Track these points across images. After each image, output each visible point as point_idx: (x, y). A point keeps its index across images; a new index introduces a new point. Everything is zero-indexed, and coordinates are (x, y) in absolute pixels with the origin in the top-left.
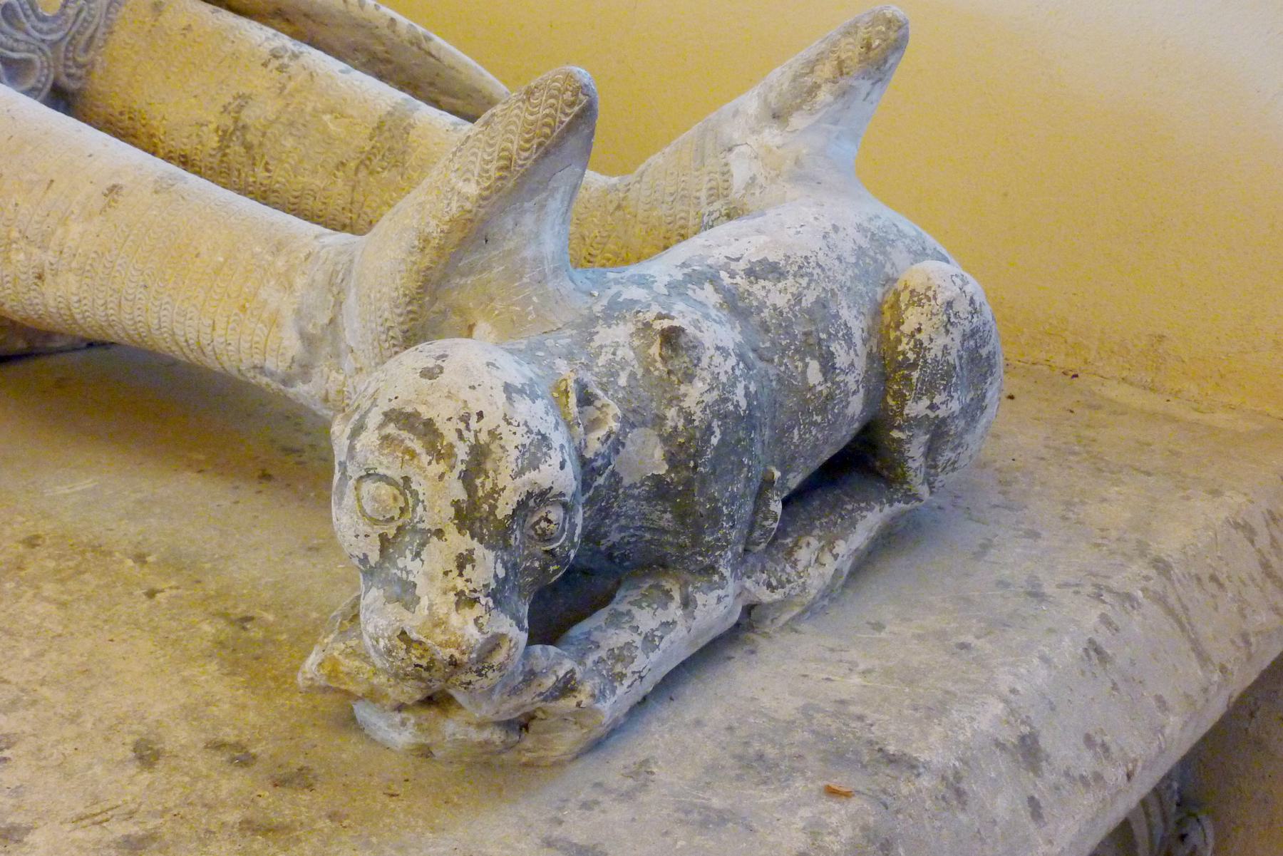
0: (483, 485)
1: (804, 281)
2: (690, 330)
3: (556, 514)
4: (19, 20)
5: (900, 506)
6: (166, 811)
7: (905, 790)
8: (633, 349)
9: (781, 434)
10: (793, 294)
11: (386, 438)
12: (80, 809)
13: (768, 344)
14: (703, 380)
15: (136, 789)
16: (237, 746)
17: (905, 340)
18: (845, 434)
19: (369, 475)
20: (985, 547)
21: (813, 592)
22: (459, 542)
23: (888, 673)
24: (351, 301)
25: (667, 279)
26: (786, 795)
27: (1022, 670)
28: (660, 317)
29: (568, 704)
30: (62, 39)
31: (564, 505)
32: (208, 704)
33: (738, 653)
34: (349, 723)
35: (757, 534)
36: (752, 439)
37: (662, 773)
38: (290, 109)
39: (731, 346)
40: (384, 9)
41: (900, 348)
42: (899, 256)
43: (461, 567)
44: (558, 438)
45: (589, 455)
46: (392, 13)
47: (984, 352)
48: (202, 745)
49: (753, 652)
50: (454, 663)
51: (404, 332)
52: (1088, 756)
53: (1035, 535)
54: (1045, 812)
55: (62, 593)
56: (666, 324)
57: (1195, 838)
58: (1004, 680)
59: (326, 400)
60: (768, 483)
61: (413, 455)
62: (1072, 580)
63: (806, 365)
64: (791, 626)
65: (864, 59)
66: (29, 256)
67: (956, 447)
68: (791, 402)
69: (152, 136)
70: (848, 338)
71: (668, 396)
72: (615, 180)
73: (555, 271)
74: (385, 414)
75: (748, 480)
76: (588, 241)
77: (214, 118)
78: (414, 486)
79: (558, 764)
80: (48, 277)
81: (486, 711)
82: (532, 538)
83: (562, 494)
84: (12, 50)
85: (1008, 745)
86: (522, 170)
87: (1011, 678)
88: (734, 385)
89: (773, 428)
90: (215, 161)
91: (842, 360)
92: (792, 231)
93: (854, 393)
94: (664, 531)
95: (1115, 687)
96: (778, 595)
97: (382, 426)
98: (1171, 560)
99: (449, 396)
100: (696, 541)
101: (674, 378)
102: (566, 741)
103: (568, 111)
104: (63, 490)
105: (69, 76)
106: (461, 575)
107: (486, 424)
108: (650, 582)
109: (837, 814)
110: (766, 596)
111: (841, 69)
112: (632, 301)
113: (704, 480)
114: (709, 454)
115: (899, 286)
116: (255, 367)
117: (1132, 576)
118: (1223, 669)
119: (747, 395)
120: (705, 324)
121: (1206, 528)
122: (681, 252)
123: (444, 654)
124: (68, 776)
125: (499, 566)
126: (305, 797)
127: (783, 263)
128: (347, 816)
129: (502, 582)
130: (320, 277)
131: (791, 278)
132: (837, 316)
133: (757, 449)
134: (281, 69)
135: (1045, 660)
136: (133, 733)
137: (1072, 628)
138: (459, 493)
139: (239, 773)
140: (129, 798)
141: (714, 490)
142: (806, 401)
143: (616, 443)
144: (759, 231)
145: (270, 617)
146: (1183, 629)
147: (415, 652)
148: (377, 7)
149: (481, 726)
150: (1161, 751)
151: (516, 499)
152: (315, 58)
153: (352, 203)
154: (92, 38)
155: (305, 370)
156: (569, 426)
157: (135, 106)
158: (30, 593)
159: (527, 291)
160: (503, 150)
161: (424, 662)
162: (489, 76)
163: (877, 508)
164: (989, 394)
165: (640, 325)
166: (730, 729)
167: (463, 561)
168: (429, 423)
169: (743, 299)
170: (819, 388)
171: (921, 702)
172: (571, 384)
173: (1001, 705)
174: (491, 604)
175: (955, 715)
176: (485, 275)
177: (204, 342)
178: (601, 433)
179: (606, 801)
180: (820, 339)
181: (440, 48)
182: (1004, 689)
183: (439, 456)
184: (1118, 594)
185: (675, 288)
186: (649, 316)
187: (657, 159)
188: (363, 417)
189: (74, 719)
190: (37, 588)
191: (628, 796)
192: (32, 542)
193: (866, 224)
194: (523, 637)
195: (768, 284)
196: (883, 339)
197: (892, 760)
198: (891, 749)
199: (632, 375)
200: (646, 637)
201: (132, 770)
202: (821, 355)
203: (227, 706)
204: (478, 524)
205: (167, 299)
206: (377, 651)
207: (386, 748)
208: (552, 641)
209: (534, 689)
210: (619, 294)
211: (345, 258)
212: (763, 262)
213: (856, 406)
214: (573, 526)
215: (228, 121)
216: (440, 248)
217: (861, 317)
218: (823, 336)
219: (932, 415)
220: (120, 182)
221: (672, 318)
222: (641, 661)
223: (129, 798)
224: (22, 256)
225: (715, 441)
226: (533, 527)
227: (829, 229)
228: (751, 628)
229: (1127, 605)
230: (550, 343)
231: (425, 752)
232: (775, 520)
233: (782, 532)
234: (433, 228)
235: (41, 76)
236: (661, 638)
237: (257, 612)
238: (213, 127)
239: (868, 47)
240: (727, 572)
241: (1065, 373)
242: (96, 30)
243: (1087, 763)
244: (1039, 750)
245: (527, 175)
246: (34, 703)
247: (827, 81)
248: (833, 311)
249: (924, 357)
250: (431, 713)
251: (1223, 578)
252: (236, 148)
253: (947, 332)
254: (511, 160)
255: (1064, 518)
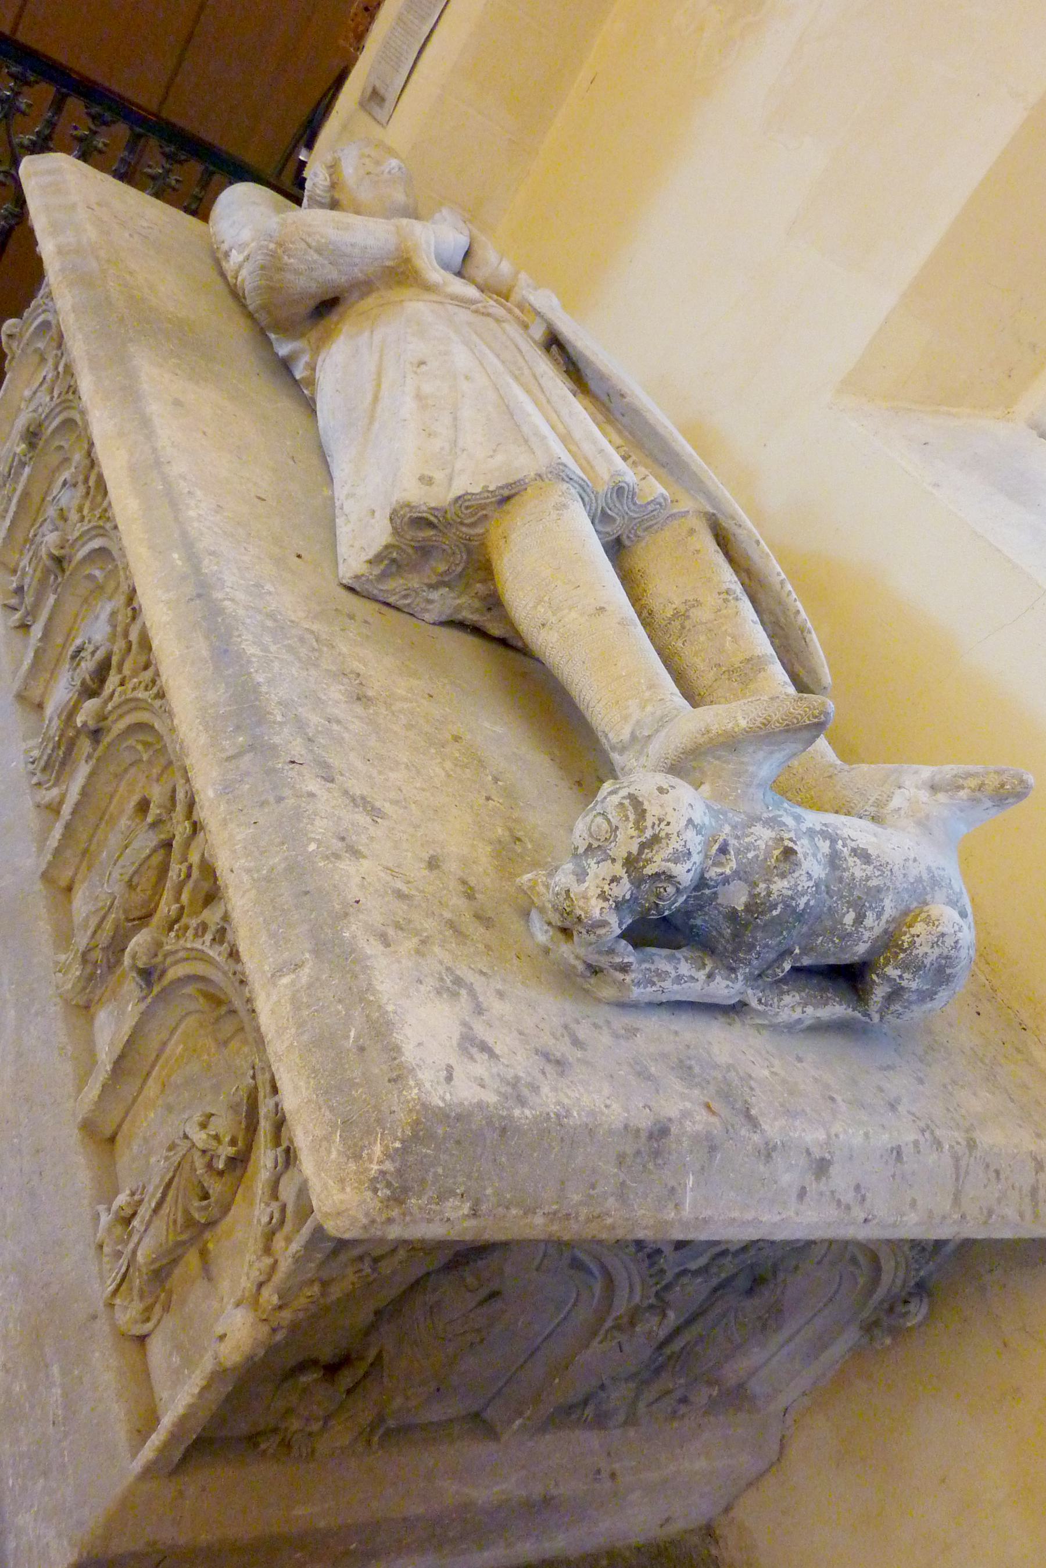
0: (647, 854)
1: (877, 873)
2: (800, 855)
3: (671, 890)
4: (623, 497)
5: (857, 1015)
6: (423, 891)
7: (743, 1132)
8: (766, 846)
9: (813, 934)
10: (867, 875)
11: (621, 804)
12: (390, 865)
13: (836, 889)
14: (789, 882)
15: (418, 874)
16: (472, 888)
17: (908, 936)
18: (846, 958)
19: (603, 814)
20: (889, 1068)
21: (780, 1020)
22: (619, 870)
23: (784, 1082)
24: (663, 734)
25: (811, 826)
26: (686, 1091)
27: (850, 1131)
28: (791, 840)
29: (620, 976)
30: (635, 519)
31: (678, 890)
32: (474, 862)
33: (722, 1019)
34: (526, 914)
35: (770, 972)
36: (795, 927)
37: (639, 1038)
38: (715, 622)
39: (815, 876)
40: (798, 603)
41: (903, 938)
42: (940, 895)
43: (612, 881)
44: (696, 858)
45: (707, 876)
46: (799, 606)
47: (948, 971)
48: (457, 877)
49: (730, 1024)
50: (579, 918)
51: (672, 765)
52: (851, 1194)
53: (921, 1081)
54: (807, 1199)
55: (452, 770)
56: (791, 845)
57: (912, 1307)
58: (837, 1128)
59: (623, 769)
60: (789, 952)
61: (627, 819)
62: (918, 1114)
63: (848, 912)
64: (759, 1028)
65: (996, 790)
66: (545, 612)
67: (905, 1007)
68: (829, 923)
69: (645, 591)
70: (879, 916)
71: (766, 877)
72: (839, 762)
73: (759, 785)
74: (629, 794)
75: (780, 943)
76: (804, 782)
77: (677, 602)
78: (618, 833)
79: (599, 1001)
80: (547, 628)
81: (582, 951)
82: (653, 891)
83: (679, 883)
84: (610, 509)
85: (813, 1156)
86: (771, 731)
87: (841, 1129)
88: (803, 895)
89: (810, 929)
90: (664, 623)
91: (870, 920)
92: (892, 846)
93: (864, 942)
94: (721, 935)
95: (893, 1176)
96: (760, 1008)
97: (624, 798)
98: (980, 1145)
99: (661, 806)
100: (735, 951)
101: (775, 871)
102: (608, 992)
103: (811, 718)
104: (487, 724)
105: (628, 537)
106: (609, 884)
107: (668, 829)
108: (701, 955)
109: (702, 1116)
110: (754, 1003)
111: (980, 787)
112: (785, 824)
113: (757, 926)
114: (768, 917)
115: (926, 909)
116: (604, 732)
117: (950, 1136)
118: (963, 1217)
119: (807, 904)
120: (810, 858)
121: (1016, 1147)
122: (830, 818)
123: (579, 912)
124: (396, 848)
125: (629, 892)
126: (482, 930)
127: (874, 857)
128: (492, 951)
129: (625, 901)
130: (659, 713)
131: (872, 867)
132: (882, 900)
133: (795, 933)
134: (725, 601)
135: (866, 1135)
136: (434, 851)
137: (896, 1133)
138: (635, 850)
139: (464, 900)
140: (412, 875)
141: (759, 935)
142: (836, 929)
143: (726, 881)
144: (875, 835)
145: (530, 846)
146: (957, 1179)
147: (568, 903)
148: (795, 600)
149: (577, 957)
150: (894, 1225)
151: (657, 870)
152: (746, 606)
153: (710, 687)
154: (651, 526)
155: (623, 749)
156: (706, 856)
157: (647, 571)
158: (439, 760)
159: (738, 785)
160: (769, 716)
161: (568, 910)
162: (827, 670)
163: (844, 1006)
164: (940, 994)
165: (778, 836)
166: (688, 1047)
167: (615, 879)
168: (644, 811)
169: (840, 860)
170: (847, 927)
171: (787, 1105)
172: (721, 839)
173: (824, 1137)
174: (613, 906)
175: (797, 1123)
176: (724, 765)
177: (591, 705)
178: (719, 870)
179: (605, 1030)
180: (864, 905)
181: (812, 640)
182: (833, 1131)
183: (638, 828)
184: (935, 1138)
185: (811, 833)
186: (786, 836)
187: (865, 767)
188: (620, 788)
189: (417, 827)
190: (444, 760)
191: (616, 1036)
192: (457, 739)
193: (933, 869)
194: (619, 931)
195: (858, 861)
196: (899, 927)
197: (749, 1117)
198: (753, 1112)
199: (757, 856)
200: (679, 976)
201: (423, 865)
202: (859, 913)
203: (481, 869)
204: (632, 868)
205: (588, 674)
206: (553, 890)
207: (532, 936)
208: (635, 946)
209: (609, 959)
210: (781, 816)
211: (675, 712)
212: (864, 850)
213: (861, 949)
214: (675, 901)
215: (682, 609)
216: (711, 739)
217: (894, 910)
218: (867, 904)
219: (898, 981)
220: (607, 608)
221: (796, 844)
222: (667, 984)
223: (412, 875)
224: (543, 610)
225: (774, 913)
226: (657, 888)
227: (912, 856)
228: (737, 1013)
229: (935, 1146)
230: (730, 815)
231: (547, 951)
232: (782, 972)
233: (783, 980)
234: (715, 728)
235: (613, 530)
236: (685, 982)
237: (526, 840)
238: (674, 606)
239: (1002, 786)
240: (740, 978)
241: (1020, 1024)
242: (656, 524)
243: (848, 1197)
244: (827, 1171)
245: (773, 734)
246: (406, 808)
247: (970, 788)
248: (881, 897)
249: (912, 950)
250: (560, 936)
251: (1003, 1176)
252: (677, 624)
253: (932, 947)
254: (769, 722)
255: (945, 1086)
